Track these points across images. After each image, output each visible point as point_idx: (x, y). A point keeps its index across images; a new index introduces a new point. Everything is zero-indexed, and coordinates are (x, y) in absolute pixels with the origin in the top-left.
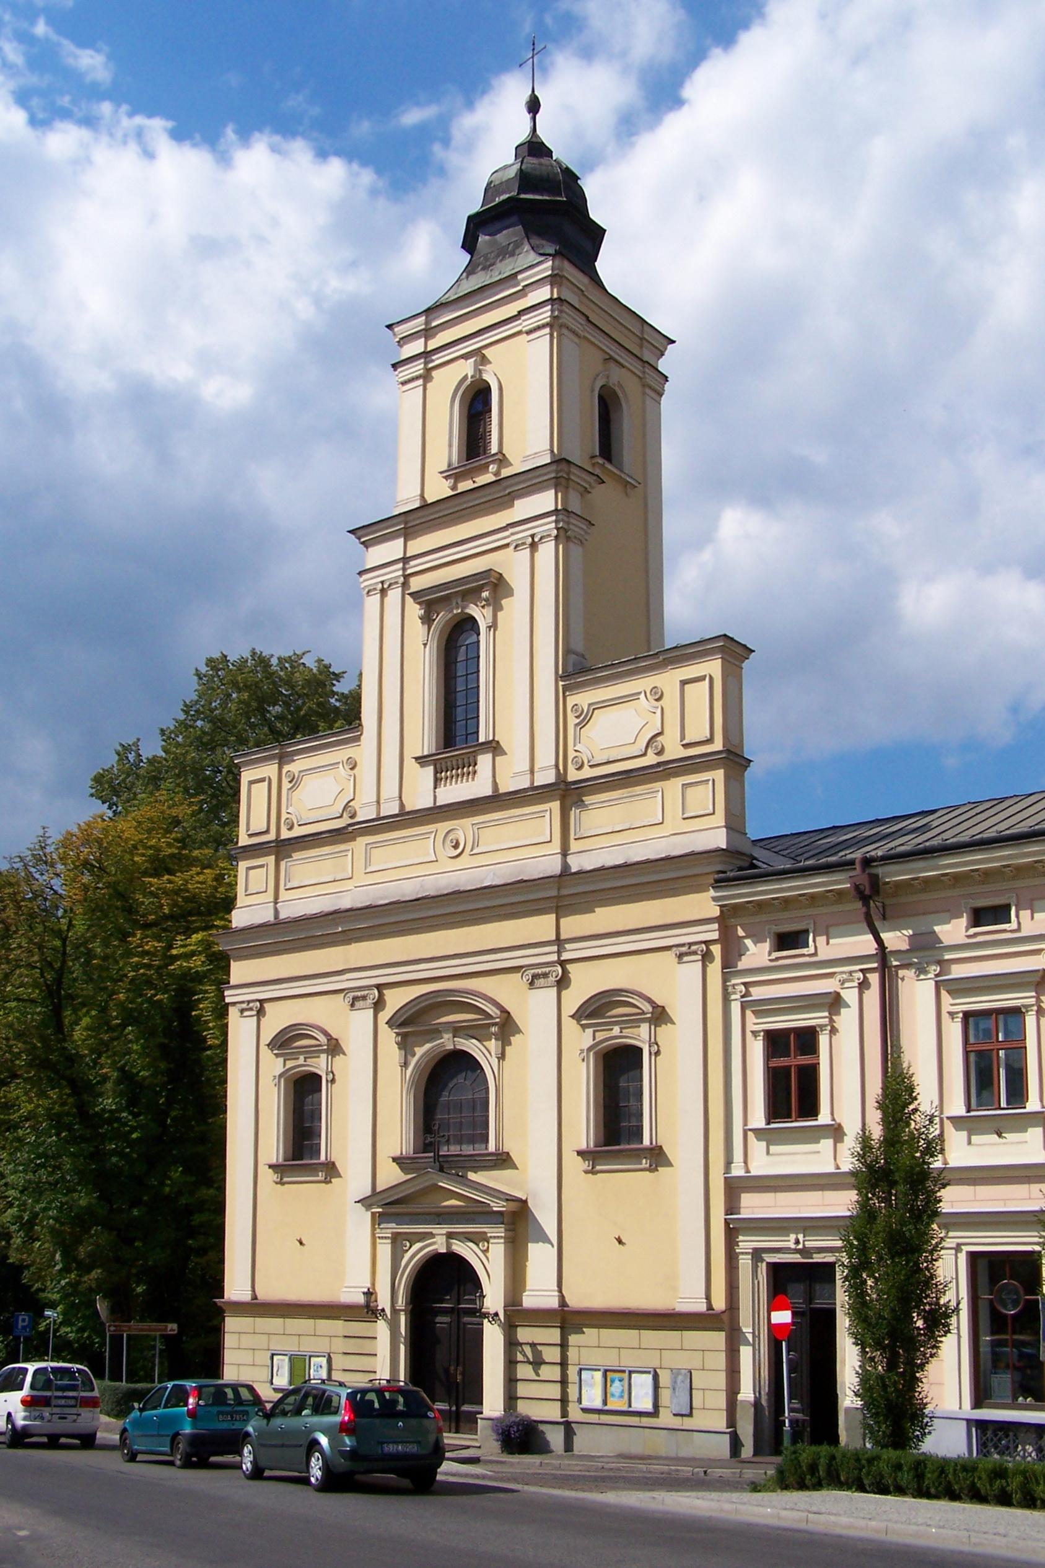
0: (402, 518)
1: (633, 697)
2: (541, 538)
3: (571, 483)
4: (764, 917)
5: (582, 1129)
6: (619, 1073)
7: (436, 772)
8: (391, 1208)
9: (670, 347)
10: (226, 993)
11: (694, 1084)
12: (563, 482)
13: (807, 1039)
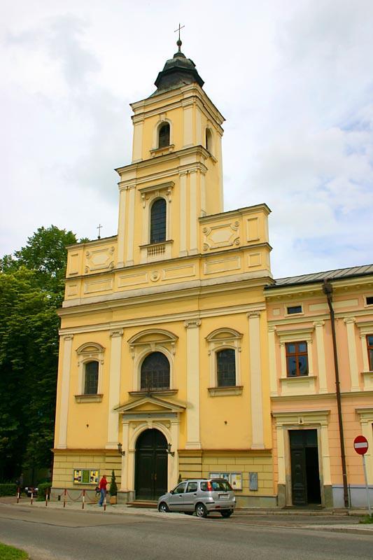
0: (197, 148)
1: (229, 225)
4: (282, 302)
5: (80, 390)
6: (226, 360)
8: (128, 413)
9: (224, 122)
11: (261, 360)
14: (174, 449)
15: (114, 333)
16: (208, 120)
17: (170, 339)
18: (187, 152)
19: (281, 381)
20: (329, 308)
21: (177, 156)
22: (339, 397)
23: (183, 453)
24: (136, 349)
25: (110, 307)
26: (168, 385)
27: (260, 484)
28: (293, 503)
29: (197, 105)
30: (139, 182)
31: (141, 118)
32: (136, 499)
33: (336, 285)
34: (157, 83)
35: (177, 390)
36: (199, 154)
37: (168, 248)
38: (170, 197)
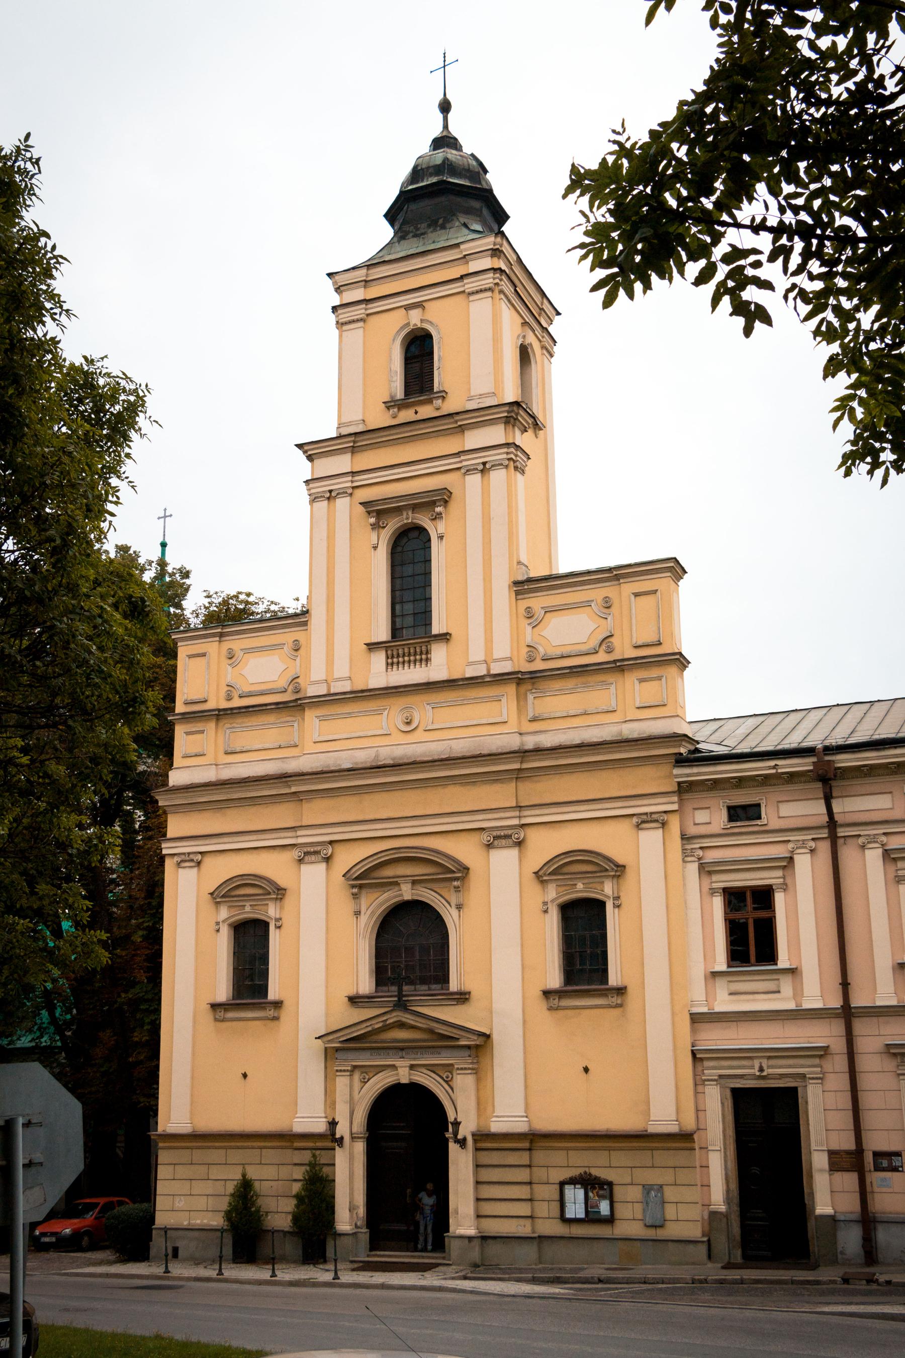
0: (507, 408)
1: (587, 604)
2: (493, 466)
3: (517, 423)
7: (387, 658)
8: (346, 1047)
10: (163, 846)
11: (667, 927)
12: (512, 420)
13: (764, 897)
14: (465, 1131)
15: (307, 854)
16: (525, 323)
17: (454, 874)
18: (481, 416)
19: (715, 974)
20: (825, 811)
21: (457, 422)
22: (847, 1014)
23: (484, 1139)
24: (364, 892)
25: (293, 789)
26: (444, 979)
27: (670, 1212)
28: (744, 1256)
29: (501, 292)
30: (361, 480)
31: (359, 312)
32: (371, 1250)
33: (845, 761)
34: (391, 216)
35: (469, 993)
36: (510, 421)
37: (438, 652)
38: (441, 527)
